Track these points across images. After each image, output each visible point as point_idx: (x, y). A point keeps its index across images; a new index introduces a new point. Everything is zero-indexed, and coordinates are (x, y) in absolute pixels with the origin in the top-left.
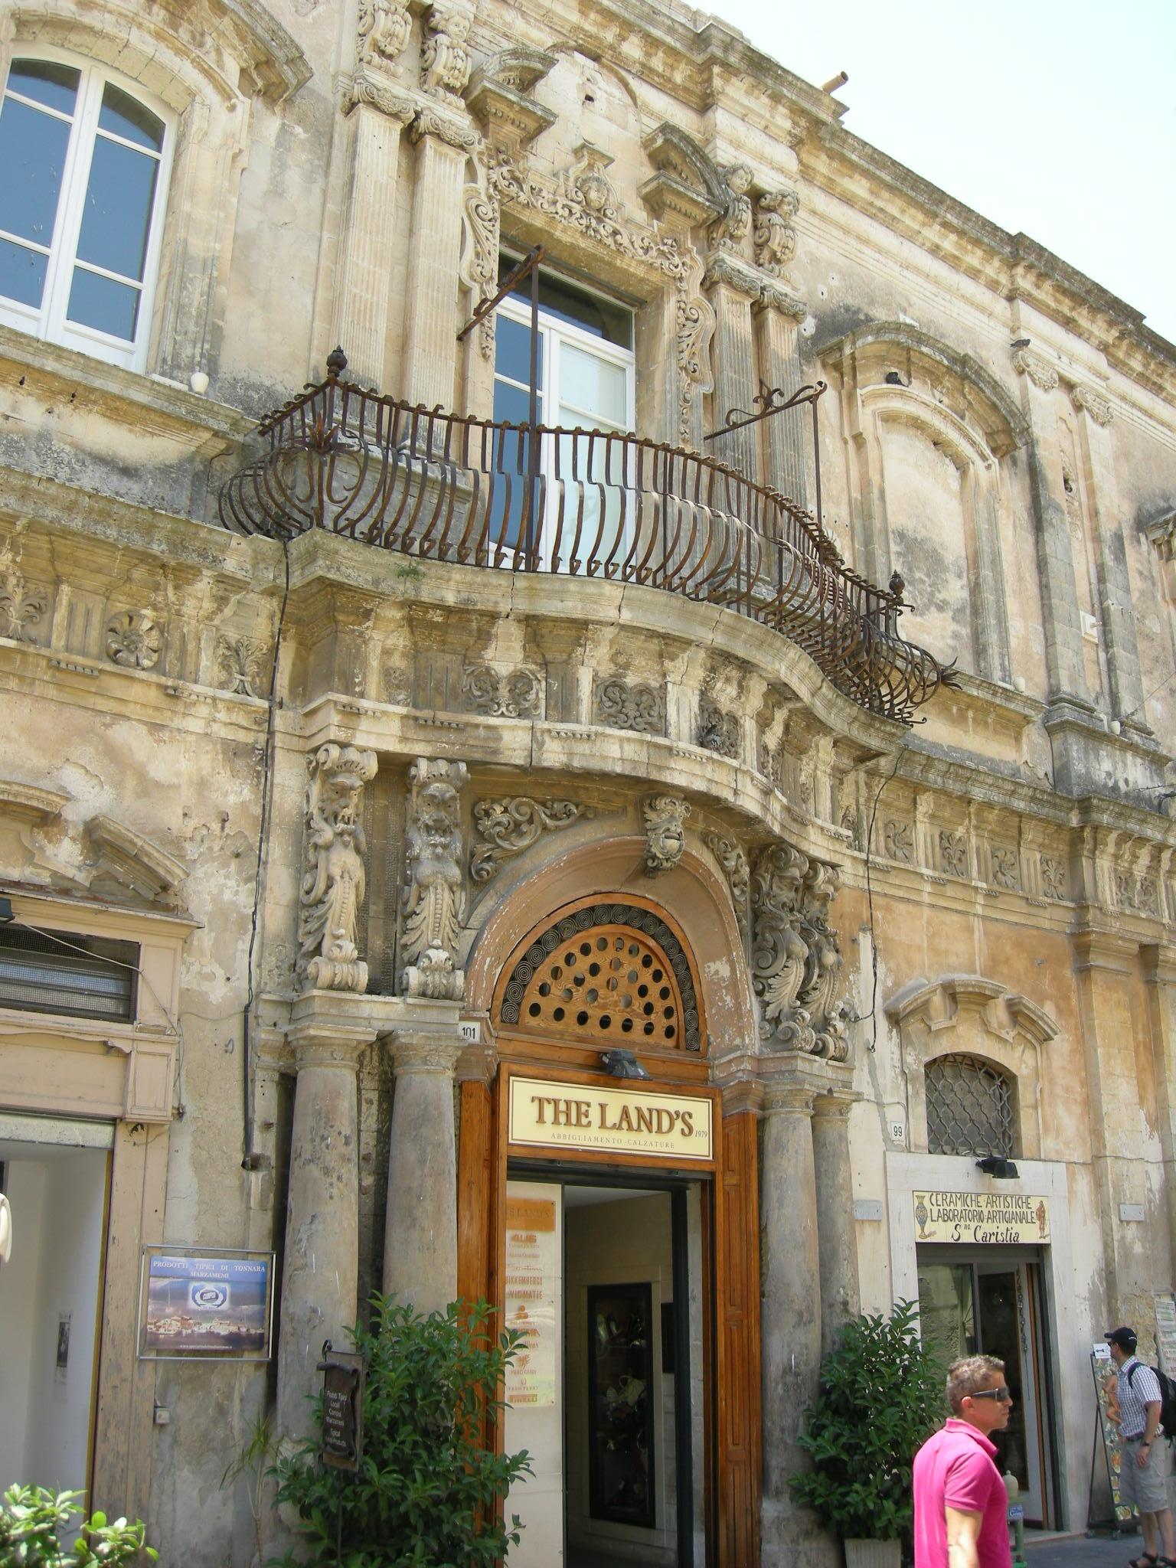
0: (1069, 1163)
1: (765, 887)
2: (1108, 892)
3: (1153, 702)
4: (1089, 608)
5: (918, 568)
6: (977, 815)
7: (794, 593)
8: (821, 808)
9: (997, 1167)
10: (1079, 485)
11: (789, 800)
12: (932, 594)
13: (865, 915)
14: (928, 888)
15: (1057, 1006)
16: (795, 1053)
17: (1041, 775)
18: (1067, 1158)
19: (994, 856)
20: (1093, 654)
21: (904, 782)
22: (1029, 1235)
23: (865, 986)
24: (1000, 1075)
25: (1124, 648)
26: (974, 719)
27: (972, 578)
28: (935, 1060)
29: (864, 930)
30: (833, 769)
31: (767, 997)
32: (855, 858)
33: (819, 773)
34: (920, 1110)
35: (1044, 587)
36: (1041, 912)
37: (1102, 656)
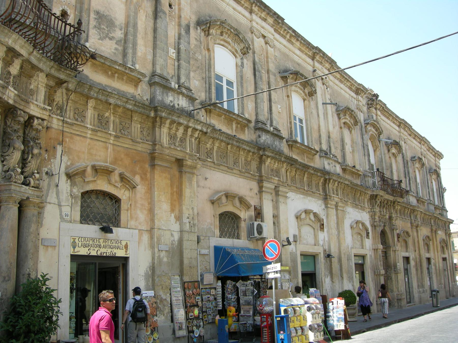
0: (140, 230)
1: (8, 123)
2: (165, 140)
3: (195, 81)
4: (173, 47)
5: (103, 24)
6: (114, 109)
7: (23, 16)
8: (39, 98)
9: (106, 230)
10: (176, 7)
11: (18, 92)
12: (108, 34)
13: (61, 139)
14: (90, 132)
15: (141, 177)
16: (11, 183)
17: (145, 99)
18: (140, 228)
19: (120, 124)
20: (173, 62)
21: (82, 95)
22: (120, 253)
23: (59, 163)
24: (115, 199)
25: (185, 62)
26: (118, 77)
27: (126, 30)
28: (88, 191)
29: (59, 144)
30: (46, 85)
31: (4, 163)
32: (58, 119)
33: (39, 86)
34: (78, 208)
35: (155, 38)
36: (138, 145)
37: (176, 64)
